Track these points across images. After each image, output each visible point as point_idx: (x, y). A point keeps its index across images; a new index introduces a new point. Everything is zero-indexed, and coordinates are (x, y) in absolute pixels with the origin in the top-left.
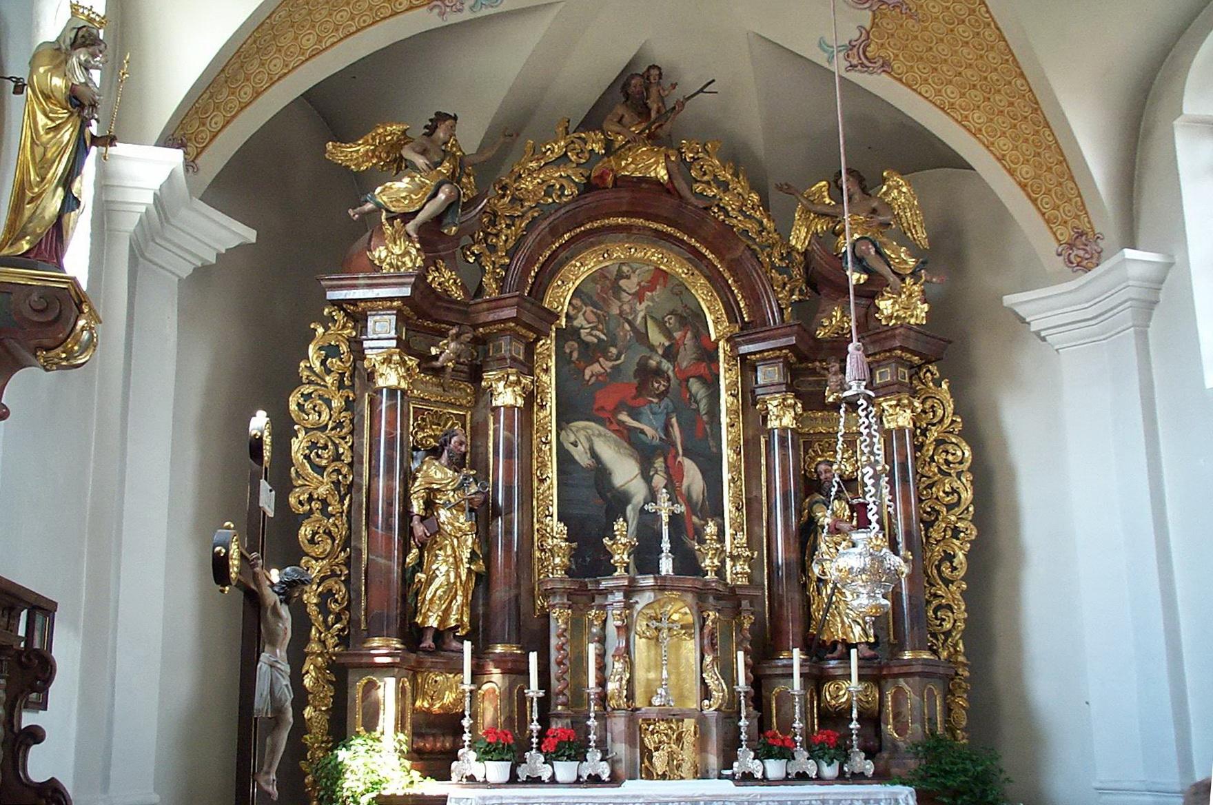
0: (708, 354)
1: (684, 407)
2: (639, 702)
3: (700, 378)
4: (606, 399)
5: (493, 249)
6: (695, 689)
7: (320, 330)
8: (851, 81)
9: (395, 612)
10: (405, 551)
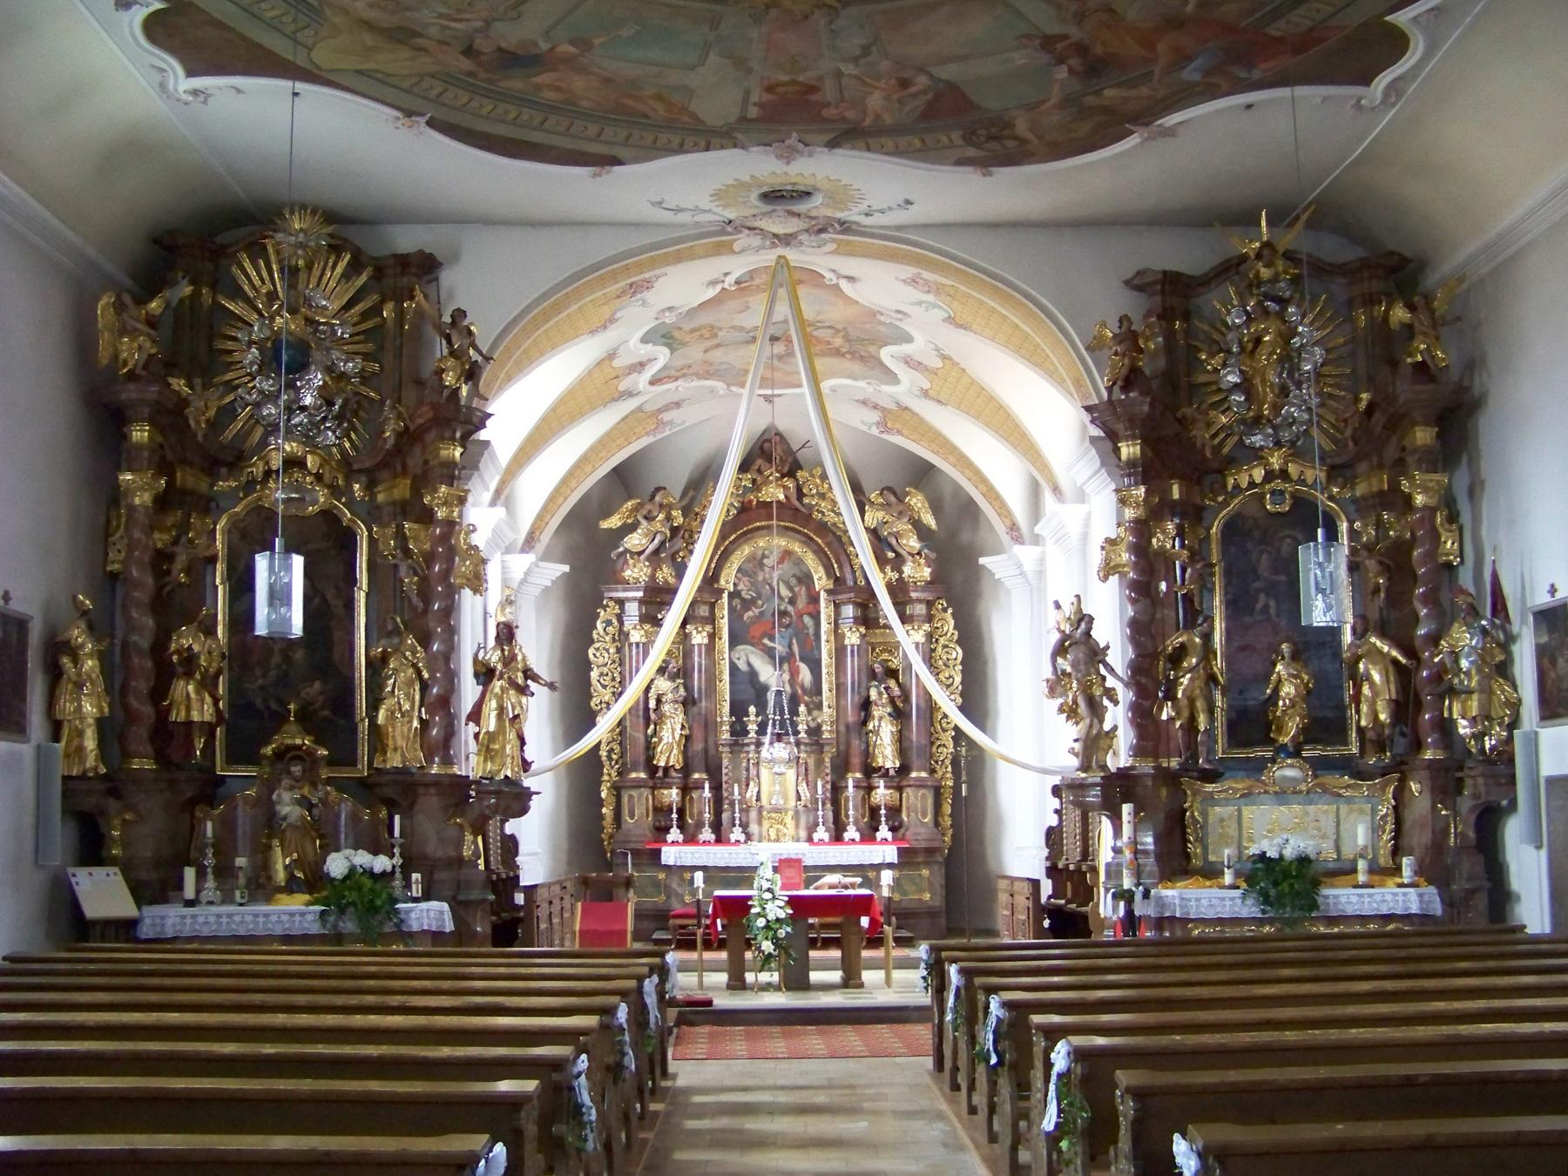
0: (814, 599)
1: (800, 633)
2: (764, 801)
3: (810, 614)
4: (756, 631)
6: (792, 795)
7: (602, 613)
9: (642, 758)
10: (647, 726)
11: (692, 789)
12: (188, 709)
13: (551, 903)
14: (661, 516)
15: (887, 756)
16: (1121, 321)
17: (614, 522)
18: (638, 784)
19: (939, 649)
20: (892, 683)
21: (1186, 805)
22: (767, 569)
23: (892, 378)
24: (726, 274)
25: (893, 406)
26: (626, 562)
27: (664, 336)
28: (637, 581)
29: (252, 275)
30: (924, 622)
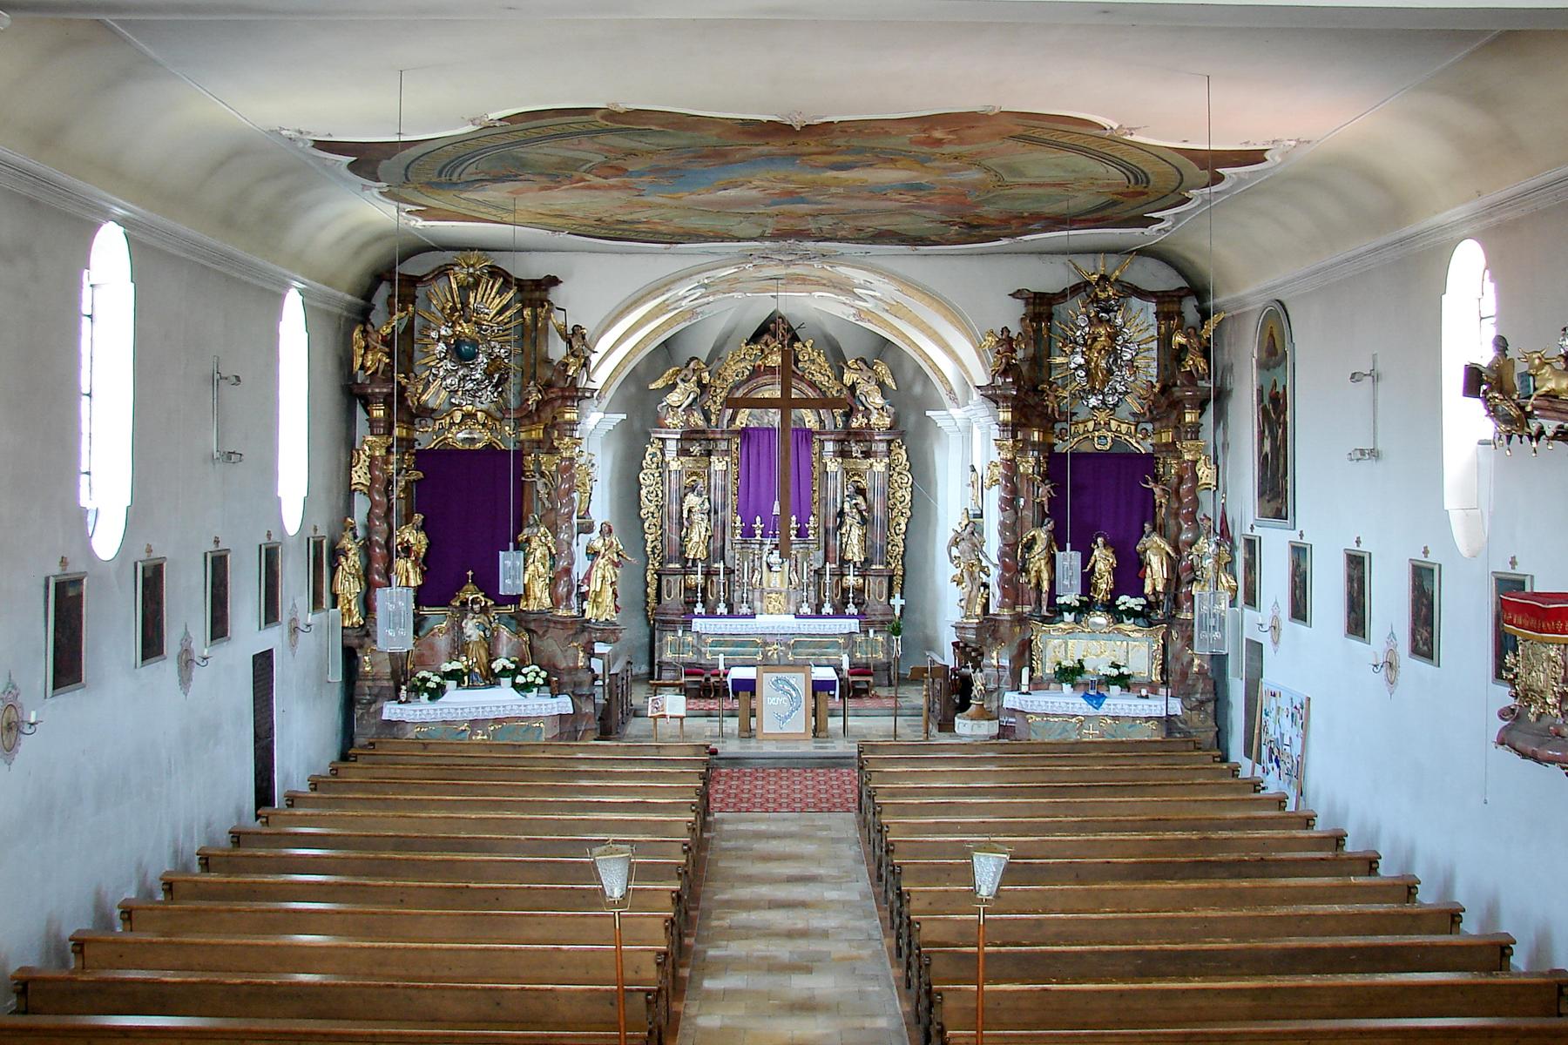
2: (765, 585)
5: (715, 402)
8: (1278, 1019)
14: (695, 378)
15: (855, 553)
17: (660, 384)
18: (674, 573)
19: (895, 476)
20: (860, 500)
26: (668, 412)
29: (441, 294)
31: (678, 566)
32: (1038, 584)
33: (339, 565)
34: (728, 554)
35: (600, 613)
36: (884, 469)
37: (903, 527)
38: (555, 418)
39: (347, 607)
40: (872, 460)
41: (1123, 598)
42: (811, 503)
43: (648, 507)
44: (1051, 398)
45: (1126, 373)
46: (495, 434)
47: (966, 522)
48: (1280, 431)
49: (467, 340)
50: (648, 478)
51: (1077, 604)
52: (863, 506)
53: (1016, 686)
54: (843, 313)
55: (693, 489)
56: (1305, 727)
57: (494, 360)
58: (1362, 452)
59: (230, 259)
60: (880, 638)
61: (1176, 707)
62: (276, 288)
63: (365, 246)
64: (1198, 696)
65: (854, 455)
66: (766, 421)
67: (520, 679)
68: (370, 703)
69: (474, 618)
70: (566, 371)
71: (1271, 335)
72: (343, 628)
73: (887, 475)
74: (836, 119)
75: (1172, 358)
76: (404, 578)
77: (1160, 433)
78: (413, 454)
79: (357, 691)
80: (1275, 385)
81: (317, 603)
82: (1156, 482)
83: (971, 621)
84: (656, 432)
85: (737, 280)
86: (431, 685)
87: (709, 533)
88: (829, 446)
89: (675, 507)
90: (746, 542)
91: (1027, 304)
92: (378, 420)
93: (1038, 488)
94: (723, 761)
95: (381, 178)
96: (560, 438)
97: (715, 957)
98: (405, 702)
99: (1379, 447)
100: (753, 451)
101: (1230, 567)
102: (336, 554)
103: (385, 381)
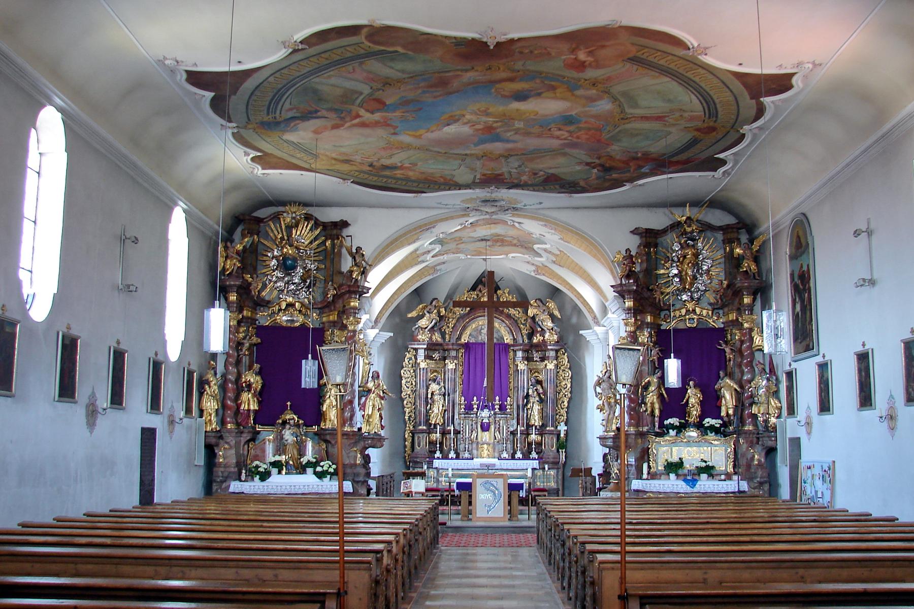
5: (448, 327)
11: (446, 434)
12: (249, 405)
13: (387, 483)
14: (435, 311)
15: (536, 420)
16: (626, 251)
17: (413, 314)
19: (561, 371)
20: (539, 387)
21: (650, 446)
22: (483, 335)
23: (540, 256)
24: (466, 222)
25: (541, 265)
27: (440, 242)
28: (424, 340)
29: (275, 231)
30: (554, 359)
31: (425, 428)
32: (653, 411)
33: (205, 391)
34: (456, 422)
35: (371, 428)
36: (553, 368)
37: (566, 404)
38: (344, 306)
39: (209, 418)
40: (546, 362)
41: (707, 420)
42: (508, 388)
43: (406, 391)
44: (658, 293)
45: (705, 277)
46: (307, 318)
47: (606, 370)
48: (806, 295)
49: (290, 257)
50: (406, 373)
51: (678, 424)
52: (541, 391)
53: (639, 476)
54: (527, 270)
55: (434, 381)
56: (832, 482)
57: (307, 272)
58: (864, 280)
59: (135, 166)
60: (552, 472)
61: (744, 486)
62: (169, 203)
63: (227, 192)
64: (758, 479)
65: (535, 359)
66: (480, 339)
67: (319, 469)
68: (222, 482)
69: (290, 429)
70: (351, 275)
71: (798, 237)
72: (206, 432)
73: (555, 372)
74: (516, 36)
75: (733, 263)
76: (247, 404)
77: (728, 314)
78: (255, 328)
79: (214, 474)
80: (802, 267)
81: (188, 411)
82: (727, 344)
83: (610, 434)
84: (412, 345)
85: (460, 240)
86: (261, 469)
87: (444, 408)
88: (520, 354)
89: (423, 391)
90: (467, 413)
91: (641, 237)
92: (233, 302)
93: (651, 351)
94: (450, 529)
95: (233, 119)
96: (348, 318)
97: (434, 594)
98: (244, 481)
99: (875, 277)
100: (472, 357)
101: (776, 394)
102: (203, 383)
103: (237, 277)
